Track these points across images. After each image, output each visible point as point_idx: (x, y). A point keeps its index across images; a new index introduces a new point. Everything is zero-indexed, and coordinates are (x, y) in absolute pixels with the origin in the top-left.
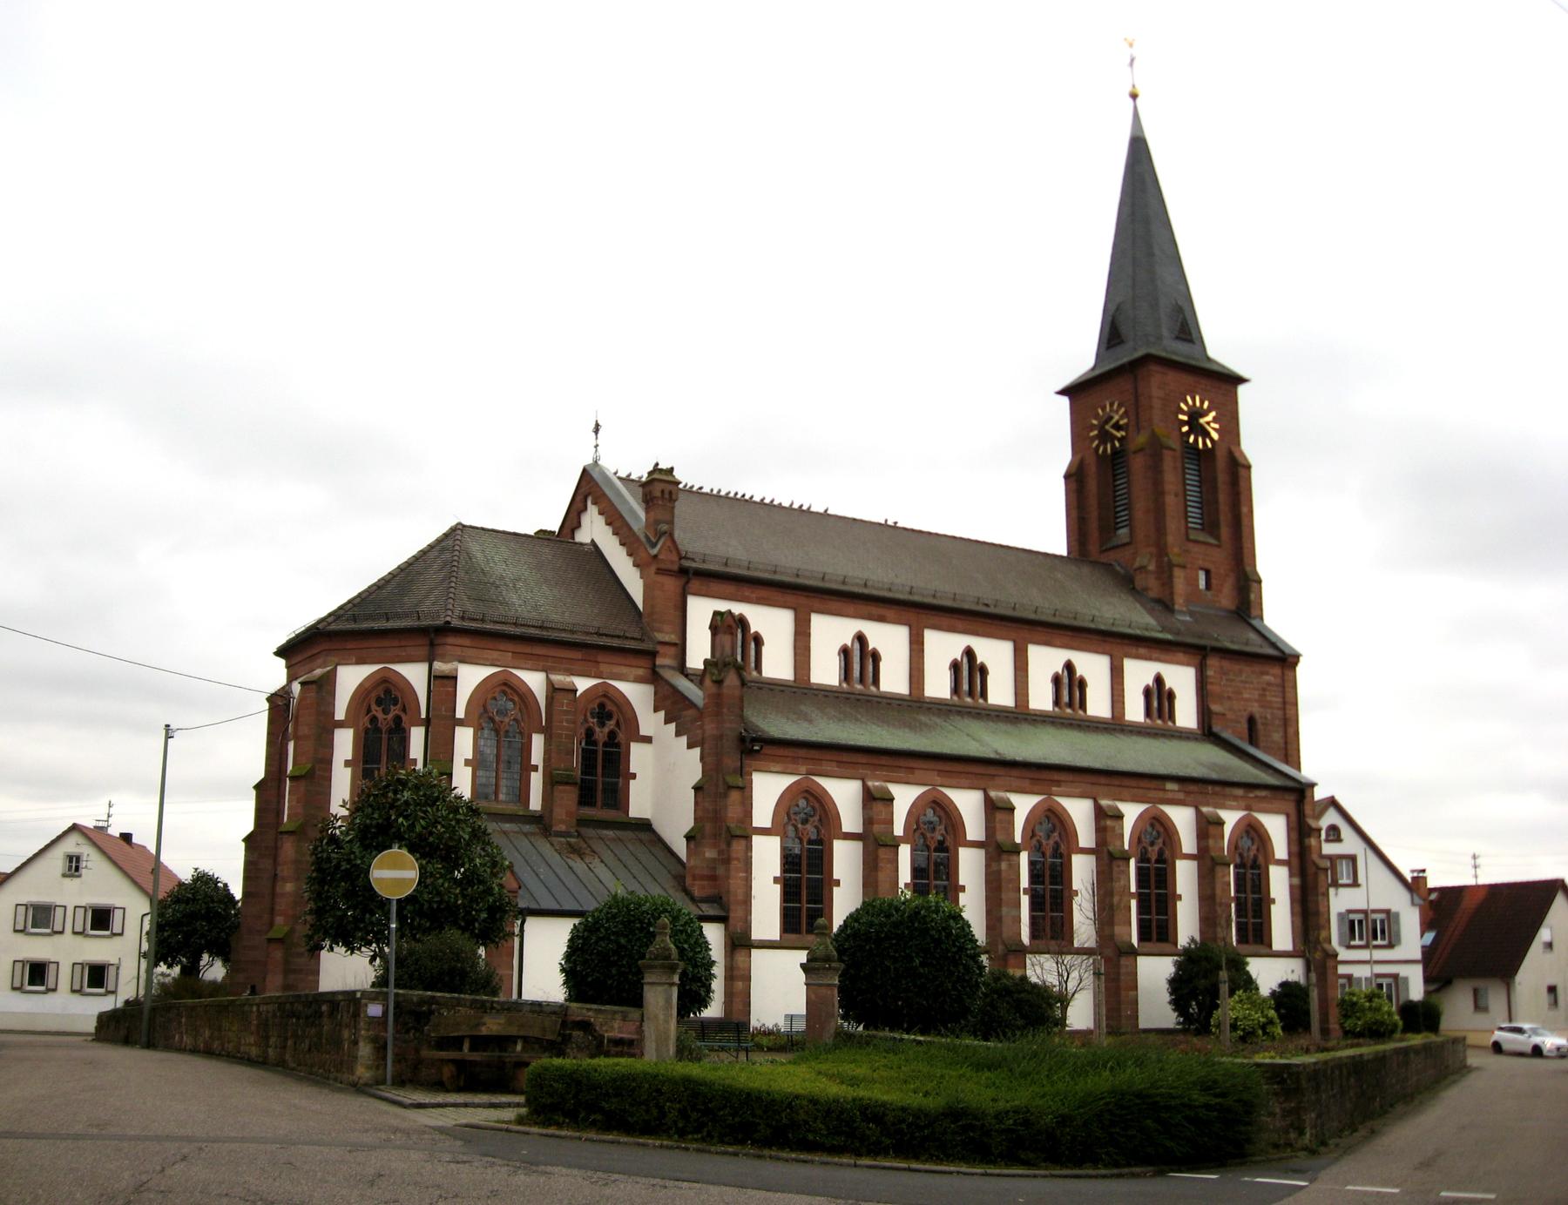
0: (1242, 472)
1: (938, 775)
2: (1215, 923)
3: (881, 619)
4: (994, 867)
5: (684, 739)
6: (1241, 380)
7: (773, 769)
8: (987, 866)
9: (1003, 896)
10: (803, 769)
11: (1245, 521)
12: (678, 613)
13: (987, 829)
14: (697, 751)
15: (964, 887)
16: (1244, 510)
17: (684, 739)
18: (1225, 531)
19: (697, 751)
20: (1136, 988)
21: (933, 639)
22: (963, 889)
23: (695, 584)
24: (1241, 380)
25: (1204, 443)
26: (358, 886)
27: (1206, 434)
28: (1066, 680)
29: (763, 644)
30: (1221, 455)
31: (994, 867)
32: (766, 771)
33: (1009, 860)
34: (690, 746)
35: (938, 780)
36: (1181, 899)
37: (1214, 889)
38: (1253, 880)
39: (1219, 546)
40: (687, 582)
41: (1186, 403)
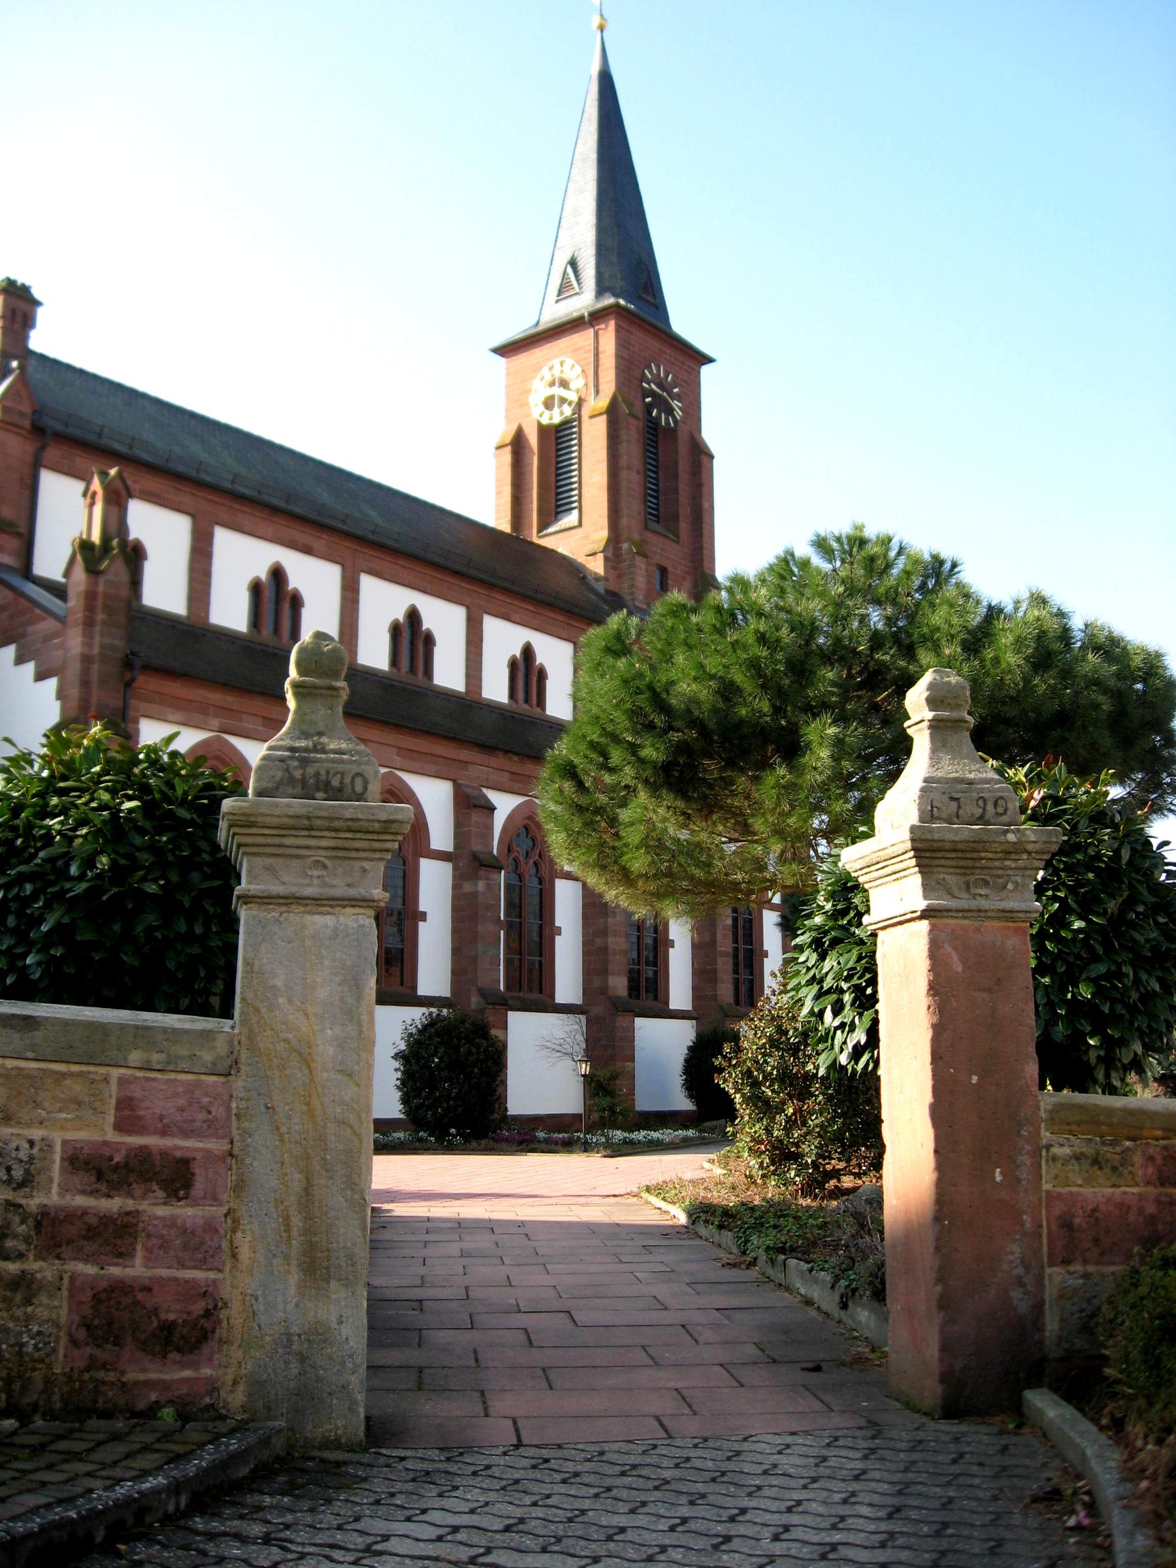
0: (704, 458)
1: (398, 755)
2: (606, 970)
3: (307, 550)
4: (467, 887)
5: (30, 668)
6: (709, 360)
7: (170, 717)
8: (456, 887)
9: (480, 928)
10: (215, 723)
11: (706, 519)
12: (27, 493)
13: (457, 835)
14: (52, 684)
15: (425, 913)
16: (706, 505)
17: (30, 668)
18: (684, 526)
19: (52, 684)
20: (632, 1059)
21: (370, 586)
22: (423, 916)
23: (53, 452)
24: (709, 360)
25: (667, 420)
26: (159, 885)
27: (670, 411)
28: (522, 667)
29: (145, 558)
30: (682, 437)
31: (467, 887)
32: (166, 721)
33: (488, 879)
34: (40, 677)
35: (398, 761)
36: (425, 920)
37: (714, 935)
38: (744, 927)
39: (678, 542)
40: (43, 448)
41: (651, 372)
